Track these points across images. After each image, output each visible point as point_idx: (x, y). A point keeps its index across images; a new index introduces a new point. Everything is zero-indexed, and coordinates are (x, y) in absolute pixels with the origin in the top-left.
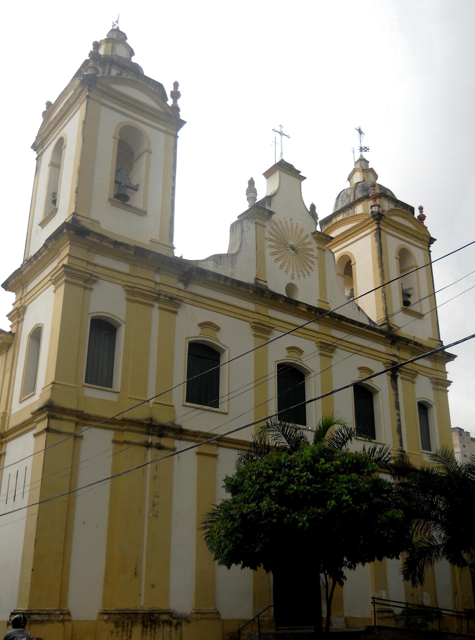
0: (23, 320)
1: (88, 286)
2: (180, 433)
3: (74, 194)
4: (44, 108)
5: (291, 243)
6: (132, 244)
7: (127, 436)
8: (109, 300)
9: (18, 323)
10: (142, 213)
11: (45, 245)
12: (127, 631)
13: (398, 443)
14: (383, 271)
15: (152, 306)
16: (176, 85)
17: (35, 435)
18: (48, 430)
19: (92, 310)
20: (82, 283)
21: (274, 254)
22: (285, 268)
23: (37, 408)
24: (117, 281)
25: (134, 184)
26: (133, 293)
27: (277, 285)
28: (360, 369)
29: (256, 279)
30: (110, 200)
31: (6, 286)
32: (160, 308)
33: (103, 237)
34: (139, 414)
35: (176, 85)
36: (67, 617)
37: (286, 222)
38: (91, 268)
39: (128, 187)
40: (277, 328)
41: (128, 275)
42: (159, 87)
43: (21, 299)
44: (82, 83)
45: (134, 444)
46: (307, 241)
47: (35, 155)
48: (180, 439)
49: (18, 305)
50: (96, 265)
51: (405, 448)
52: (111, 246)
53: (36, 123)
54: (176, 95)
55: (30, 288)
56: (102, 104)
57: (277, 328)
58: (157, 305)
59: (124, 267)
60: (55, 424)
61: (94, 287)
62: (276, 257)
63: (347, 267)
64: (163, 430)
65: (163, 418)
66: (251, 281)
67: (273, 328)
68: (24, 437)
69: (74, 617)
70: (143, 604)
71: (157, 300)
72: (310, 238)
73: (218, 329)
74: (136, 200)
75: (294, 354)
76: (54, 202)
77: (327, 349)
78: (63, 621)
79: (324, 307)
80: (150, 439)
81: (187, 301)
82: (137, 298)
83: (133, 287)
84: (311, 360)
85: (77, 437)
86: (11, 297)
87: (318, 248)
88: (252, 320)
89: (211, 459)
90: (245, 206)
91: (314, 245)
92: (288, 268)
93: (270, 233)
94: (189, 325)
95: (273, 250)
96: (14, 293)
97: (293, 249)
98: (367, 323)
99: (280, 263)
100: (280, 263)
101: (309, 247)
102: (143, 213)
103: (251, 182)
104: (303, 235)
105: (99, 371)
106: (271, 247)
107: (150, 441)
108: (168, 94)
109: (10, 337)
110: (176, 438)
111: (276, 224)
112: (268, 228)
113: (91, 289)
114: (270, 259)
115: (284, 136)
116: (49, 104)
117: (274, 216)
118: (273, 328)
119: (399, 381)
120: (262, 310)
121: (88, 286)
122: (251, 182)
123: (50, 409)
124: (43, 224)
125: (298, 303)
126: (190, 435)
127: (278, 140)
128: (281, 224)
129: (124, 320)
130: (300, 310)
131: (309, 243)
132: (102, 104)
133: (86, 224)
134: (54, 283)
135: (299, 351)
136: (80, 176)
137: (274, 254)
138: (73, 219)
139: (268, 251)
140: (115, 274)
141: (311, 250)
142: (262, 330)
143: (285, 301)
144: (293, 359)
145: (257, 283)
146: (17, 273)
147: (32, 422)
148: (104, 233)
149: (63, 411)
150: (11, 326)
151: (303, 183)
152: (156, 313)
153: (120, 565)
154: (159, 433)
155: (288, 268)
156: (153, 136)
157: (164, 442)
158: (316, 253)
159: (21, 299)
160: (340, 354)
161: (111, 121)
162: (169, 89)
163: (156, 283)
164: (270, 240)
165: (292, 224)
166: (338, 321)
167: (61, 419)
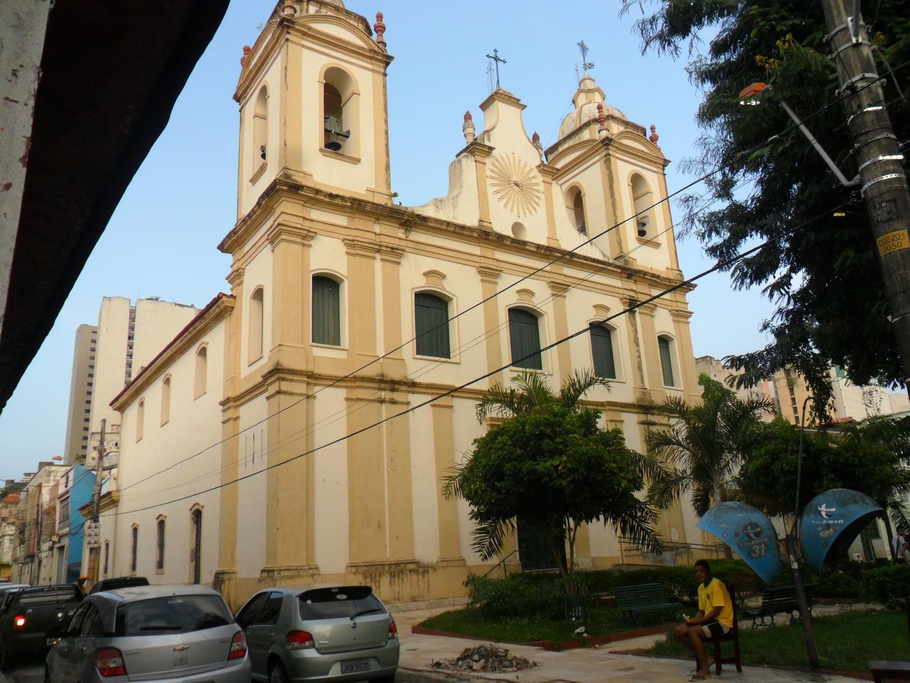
0: (242, 282)
1: (306, 242)
2: (413, 386)
5: (514, 179)
6: (347, 195)
8: (328, 255)
15: (374, 258)
16: (380, 17)
19: (311, 269)
20: (299, 240)
21: (497, 192)
28: (594, 306)
32: (382, 260)
33: (318, 192)
34: (372, 371)
35: (380, 17)
36: (315, 571)
37: (508, 157)
38: (307, 224)
40: (505, 271)
42: (363, 20)
46: (531, 175)
47: (237, 106)
49: (235, 268)
50: (312, 221)
51: (647, 386)
52: (327, 200)
54: (380, 29)
56: (303, 46)
57: (505, 271)
58: (378, 256)
60: (285, 386)
62: (499, 196)
63: (577, 199)
64: (393, 385)
65: (394, 374)
69: (323, 570)
71: (378, 251)
72: (535, 172)
73: (443, 277)
74: (349, 147)
75: (524, 297)
77: (560, 289)
79: (553, 244)
80: (383, 394)
81: (410, 250)
83: (353, 241)
84: (541, 297)
86: (228, 258)
87: (544, 182)
88: (477, 265)
91: (540, 178)
93: (492, 171)
94: (413, 273)
95: (496, 188)
101: (534, 181)
102: (357, 161)
103: (468, 117)
104: (527, 170)
105: (326, 330)
106: (494, 185)
108: (372, 28)
111: (497, 160)
113: (310, 246)
114: (493, 199)
115: (500, 63)
116: (247, 50)
117: (494, 152)
119: (637, 315)
121: (306, 242)
122: (468, 117)
124: (254, 180)
125: (525, 243)
130: (301, 195)
131: (534, 177)
132: (303, 46)
135: (532, 294)
137: (497, 192)
139: (490, 190)
141: (537, 184)
142: (489, 274)
145: (480, 225)
148: (318, 187)
150: (232, 289)
152: (378, 265)
156: (362, 78)
157: (397, 396)
158: (541, 187)
164: (492, 178)
165: (514, 158)
166: (570, 258)
167: (292, 380)
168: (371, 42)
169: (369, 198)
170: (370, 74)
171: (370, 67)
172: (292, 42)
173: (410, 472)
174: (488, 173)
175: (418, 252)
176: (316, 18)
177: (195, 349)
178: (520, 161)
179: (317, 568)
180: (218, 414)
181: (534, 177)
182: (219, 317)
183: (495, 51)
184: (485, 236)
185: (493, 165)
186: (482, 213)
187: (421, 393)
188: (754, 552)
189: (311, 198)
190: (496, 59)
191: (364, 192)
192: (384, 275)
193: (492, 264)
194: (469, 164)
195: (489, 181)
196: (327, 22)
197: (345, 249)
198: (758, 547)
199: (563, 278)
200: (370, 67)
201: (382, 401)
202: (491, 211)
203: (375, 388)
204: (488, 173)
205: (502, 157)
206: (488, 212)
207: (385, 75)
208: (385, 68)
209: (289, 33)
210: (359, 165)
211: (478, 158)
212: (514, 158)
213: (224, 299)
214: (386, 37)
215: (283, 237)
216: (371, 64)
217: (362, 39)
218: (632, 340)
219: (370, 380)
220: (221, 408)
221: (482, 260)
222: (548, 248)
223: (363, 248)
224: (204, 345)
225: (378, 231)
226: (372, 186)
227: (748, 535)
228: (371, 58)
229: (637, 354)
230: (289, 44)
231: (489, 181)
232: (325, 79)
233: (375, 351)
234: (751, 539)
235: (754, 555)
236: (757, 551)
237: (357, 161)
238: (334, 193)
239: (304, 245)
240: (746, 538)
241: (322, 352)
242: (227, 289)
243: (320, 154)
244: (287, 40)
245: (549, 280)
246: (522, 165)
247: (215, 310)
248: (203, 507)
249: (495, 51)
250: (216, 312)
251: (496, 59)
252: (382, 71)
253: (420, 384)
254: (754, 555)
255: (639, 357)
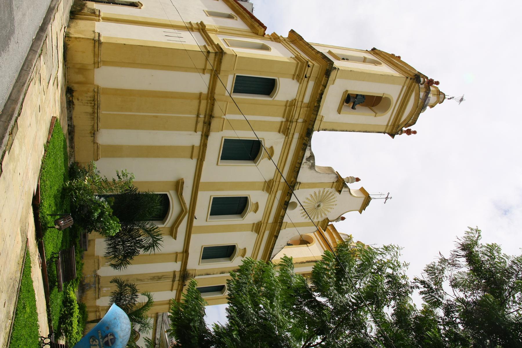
0: (272, 41)
1: (295, 77)
2: (206, 136)
3: (350, 70)
4: (396, 55)
5: (322, 205)
7: (204, 103)
8: (287, 90)
9: (270, 39)
10: (339, 111)
11: (318, 52)
12: (88, 103)
13: (200, 273)
14: (305, 263)
15: (283, 117)
16: (415, 132)
17: (205, 46)
18: (208, 52)
19: (280, 79)
20: (297, 73)
21: (315, 193)
22: (307, 201)
23: (222, 47)
24: (298, 95)
25: (356, 107)
26: (291, 105)
27: (300, 195)
28: (245, 249)
29: (300, 183)
30: (347, 91)
31: (292, 32)
32: (282, 122)
33: (325, 86)
34: (217, 111)
35: (415, 132)
36: (96, 65)
37: (334, 201)
39: (354, 103)
40: (270, 196)
41: (302, 102)
42: (414, 123)
43: (285, 40)
44: (416, 75)
45: (199, 106)
46: (323, 215)
47: (369, 49)
48: (202, 135)
49: (281, 38)
52: (319, 92)
53: (388, 50)
54: (409, 132)
55: (291, 45)
56: (403, 87)
57: (270, 196)
58: (284, 120)
59: (307, 100)
60: (212, 56)
61: (295, 81)
62: (313, 195)
63: (304, 241)
64: (208, 124)
65: (215, 123)
66: (298, 180)
67: (270, 194)
68: (203, 41)
69: (96, 71)
70: (103, 112)
71: (287, 120)
72: (324, 217)
74: (347, 108)
75: (254, 207)
76: (343, 59)
77: (257, 228)
78: (94, 63)
79: (284, 225)
80: (202, 116)
81: (287, 139)
82: (288, 108)
84: (251, 217)
85: (204, 71)
86: (286, 35)
87: (319, 222)
88: (275, 179)
89: (190, 155)
90: (344, 176)
91: (320, 219)
92: (306, 203)
93: (327, 192)
94: (272, 140)
95: (317, 193)
96: (287, 36)
97: (319, 206)
98: (273, 254)
99: (310, 198)
100: (310, 198)
101: (319, 216)
103: (358, 180)
104: (326, 212)
106: (319, 192)
107: (201, 116)
108: (409, 128)
109: (262, 34)
110: (202, 132)
111: (333, 195)
112: (330, 190)
113: (293, 79)
114: (312, 191)
115: (385, 200)
116: (399, 57)
117: (338, 193)
118: (270, 194)
120: (281, 187)
121: (295, 77)
122: (358, 180)
123: (220, 53)
124: (330, 52)
125: (285, 209)
126: (204, 141)
127: (382, 197)
128: (333, 199)
129: (275, 99)
131: (322, 216)
132: (403, 87)
133: (333, 74)
134: (296, 57)
135: (256, 211)
136: (361, 72)
137: (315, 193)
138: (335, 68)
139: (317, 190)
140: (272, 201)
141: (318, 218)
142: (269, 186)
143: (286, 202)
144: (251, 207)
145: (297, 183)
146: (301, 38)
147: (212, 45)
148: (327, 87)
149: (220, 62)
150: (268, 35)
151: (358, 212)
152: (279, 119)
153: (126, 96)
154: (207, 124)
155: (306, 203)
156: (384, 119)
157: (200, 125)
158: (315, 220)
159: (285, 40)
160: (254, 236)
161: (393, 92)
162: (412, 128)
163: (297, 119)
164: (323, 192)
165: (333, 205)
166: (274, 236)
167: (215, 60)
168: (402, 126)
169: (318, 118)
170: (386, 124)
171: (390, 124)
172: (406, 80)
173: (154, 129)
174: (326, 190)
175: (285, 144)
176: (418, 95)
177: (233, 13)
178: (331, 208)
179: (98, 67)
180: (195, 21)
181: (322, 216)
182: (252, 27)
183: (391, 198)
184: (291, 185)
185: (331, 193)
186: (305, 184)
187: (201, 140)
188: (94, 340)
189: (321, 82)
190: (387, 198)
191: (321, 115)
192: (273, 122)
193: (274, 189)
194: (332, 179)
195: (322, 190)
196: (415, 102)
197: (290, 100)
198: (98, 343)
199: (263, 231)
200: (390, 124)
201: (198, 116)
202: (305, 190)
203: (206, 112)
204: (326, 190)
205: (334, 198)
206: (304, 188)
207: (384, 133)
208: (389, 134)
209: (411, 79)
210: (336, 113)
211: (335, 184)
212: (333, 205)
213: (263, 29)
214: (405, 135)
215: (300, 63)
216: (391, 125)
217: (405, 120)
218: (223, 270)
219: (212, 110)
220: (199, 22)
221: (277, 183)
222: (281, 223)
223: (290, 111)
224: (235, 18)
225: (299, 121)
226: (324, 120)
227: (107, 336)
228: (394, 125)
229: (215, 273)
230: (405, 79)
231: (322, 190)
232: (385, 97)
233: (228, 113)
234: (103, 338)
235: (91, 340)
236: (94, 343)
237: (339, 111)
238: (323, 96)
239: (294, 75)
240: (104, 335)
241: (230, 82)
242: (268, 32)
243: (344, 90)
244: (407, 78)
245: (263, 222)
246: (329, 210)
247: (256, 25)
248: (140, 8)
249: (391, 198)
250: (256, 27)
251: (387, 198)
252: (387, 132)
253: (207, 139)
254: (91, 340)
255: (214, 274)
